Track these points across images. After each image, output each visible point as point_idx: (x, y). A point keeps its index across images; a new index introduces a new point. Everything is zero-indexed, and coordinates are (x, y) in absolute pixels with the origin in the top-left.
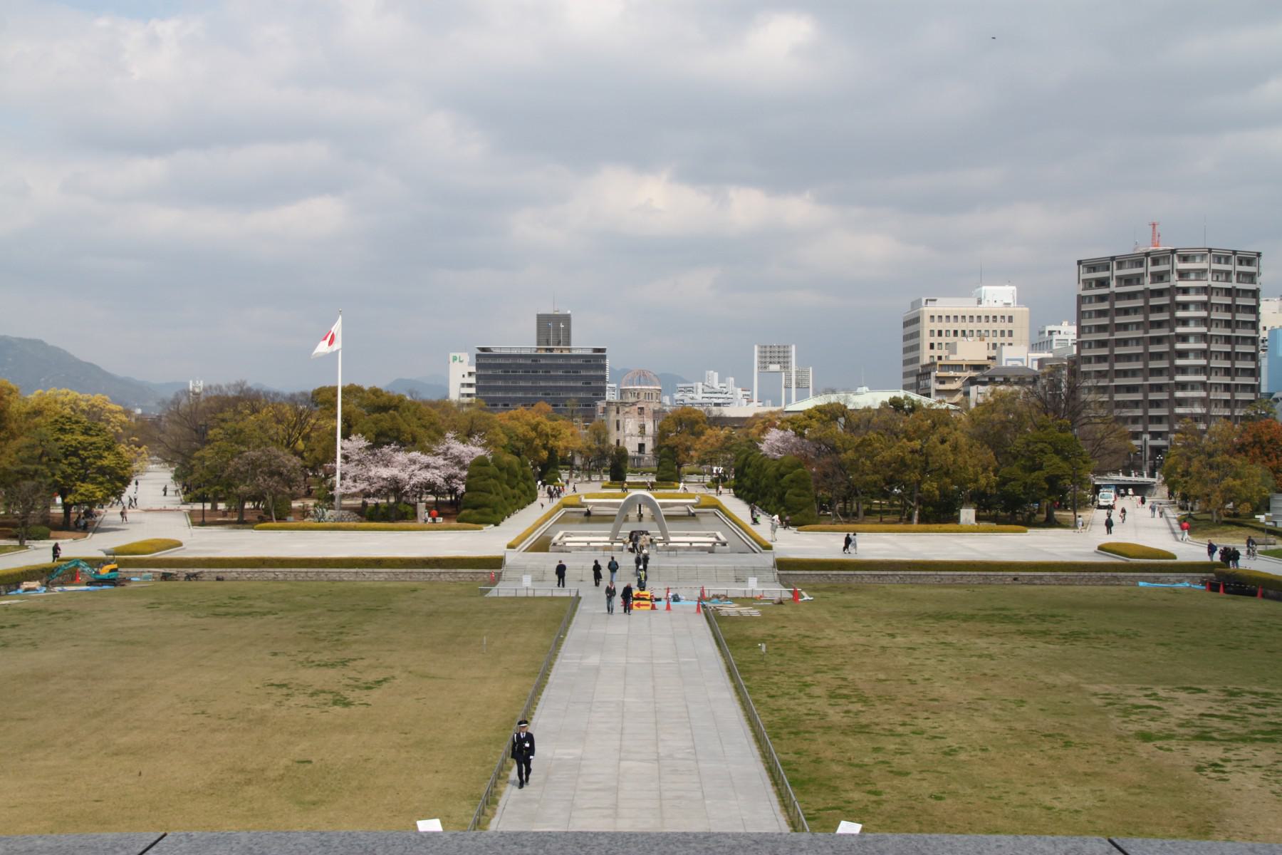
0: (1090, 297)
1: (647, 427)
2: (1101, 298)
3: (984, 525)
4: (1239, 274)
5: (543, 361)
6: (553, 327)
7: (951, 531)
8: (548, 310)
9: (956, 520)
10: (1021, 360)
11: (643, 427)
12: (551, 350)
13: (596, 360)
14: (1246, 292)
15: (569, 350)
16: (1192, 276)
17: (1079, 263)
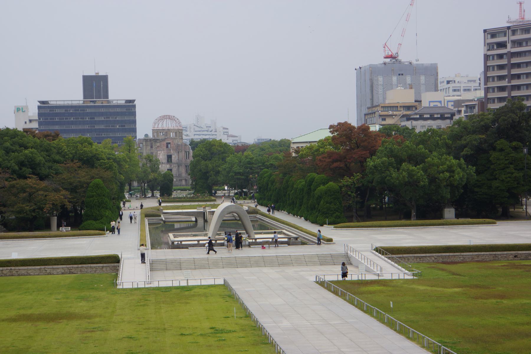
0: (493, 56)
1: (173, 157)
2: (501, 56)
3: (461, 220)
5: (88, 110)
6: (95, 85)
7: (95, 235)
9: (441, 217)
10: (440, 102)
11: (169, 157)
13: (129, 107)
15: (109, 102)
16: (524, 44)
17: (485, 31)
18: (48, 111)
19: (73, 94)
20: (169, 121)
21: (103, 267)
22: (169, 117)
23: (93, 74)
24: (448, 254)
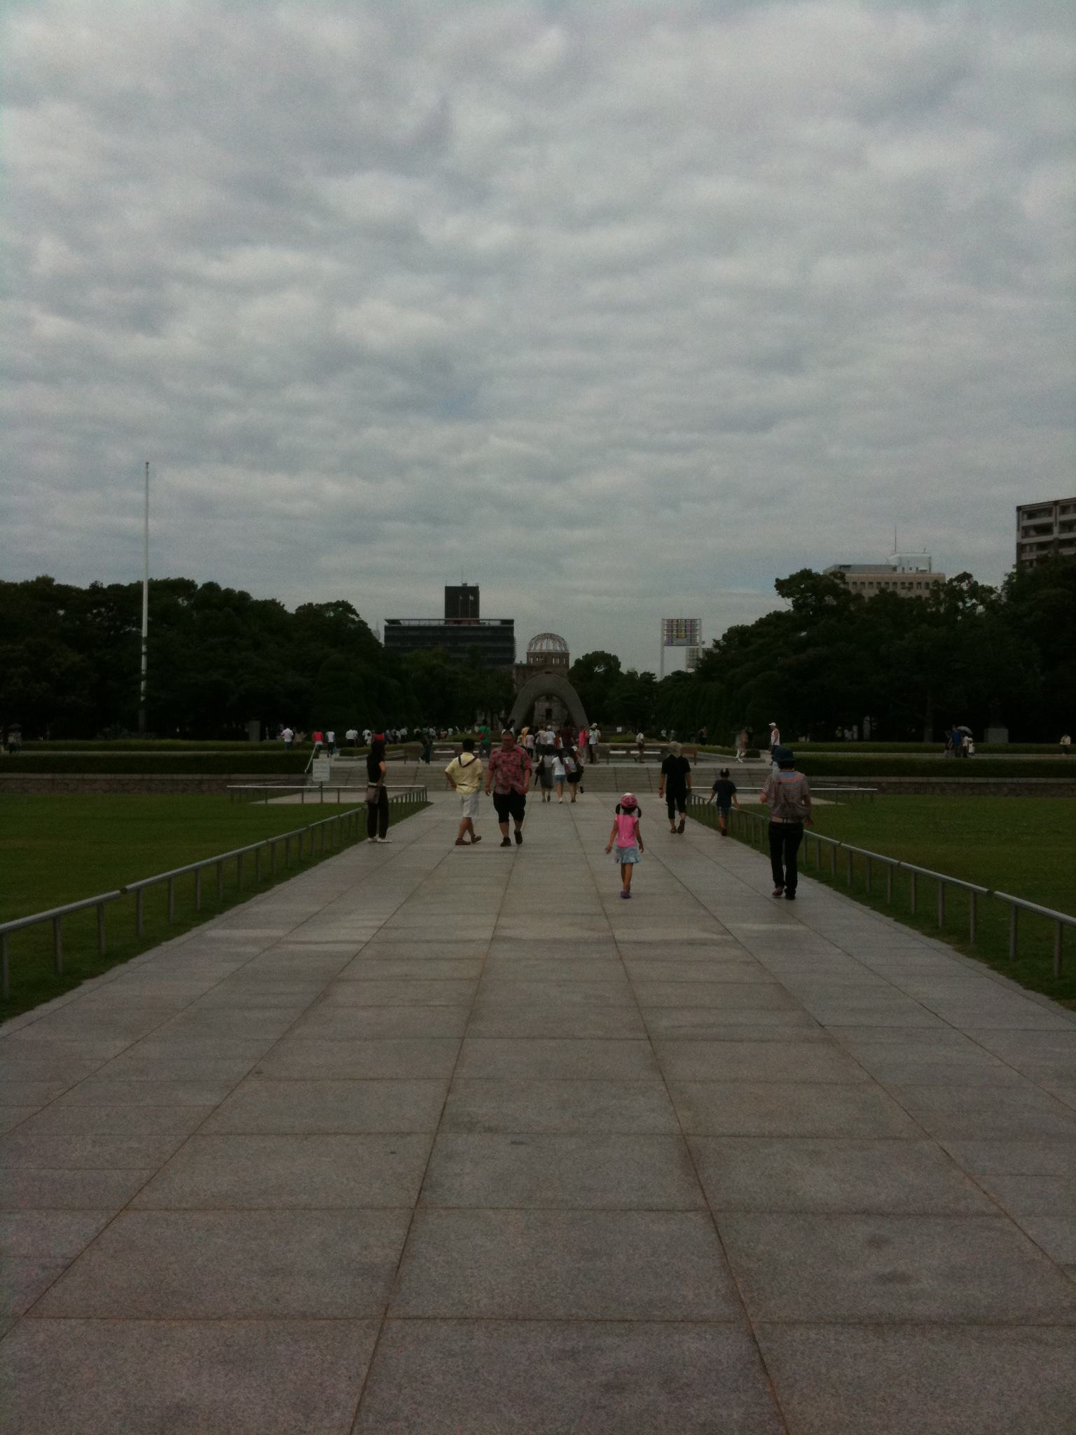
0: (1031, 545)
2: (1042, 546)
6: (462, 600)
13: (508, 625)
17: (1019, 509)
20: (551, 642)
21: (201, 782)
22: (551, 636)
23: (460, 585)
24: (1043, 780)
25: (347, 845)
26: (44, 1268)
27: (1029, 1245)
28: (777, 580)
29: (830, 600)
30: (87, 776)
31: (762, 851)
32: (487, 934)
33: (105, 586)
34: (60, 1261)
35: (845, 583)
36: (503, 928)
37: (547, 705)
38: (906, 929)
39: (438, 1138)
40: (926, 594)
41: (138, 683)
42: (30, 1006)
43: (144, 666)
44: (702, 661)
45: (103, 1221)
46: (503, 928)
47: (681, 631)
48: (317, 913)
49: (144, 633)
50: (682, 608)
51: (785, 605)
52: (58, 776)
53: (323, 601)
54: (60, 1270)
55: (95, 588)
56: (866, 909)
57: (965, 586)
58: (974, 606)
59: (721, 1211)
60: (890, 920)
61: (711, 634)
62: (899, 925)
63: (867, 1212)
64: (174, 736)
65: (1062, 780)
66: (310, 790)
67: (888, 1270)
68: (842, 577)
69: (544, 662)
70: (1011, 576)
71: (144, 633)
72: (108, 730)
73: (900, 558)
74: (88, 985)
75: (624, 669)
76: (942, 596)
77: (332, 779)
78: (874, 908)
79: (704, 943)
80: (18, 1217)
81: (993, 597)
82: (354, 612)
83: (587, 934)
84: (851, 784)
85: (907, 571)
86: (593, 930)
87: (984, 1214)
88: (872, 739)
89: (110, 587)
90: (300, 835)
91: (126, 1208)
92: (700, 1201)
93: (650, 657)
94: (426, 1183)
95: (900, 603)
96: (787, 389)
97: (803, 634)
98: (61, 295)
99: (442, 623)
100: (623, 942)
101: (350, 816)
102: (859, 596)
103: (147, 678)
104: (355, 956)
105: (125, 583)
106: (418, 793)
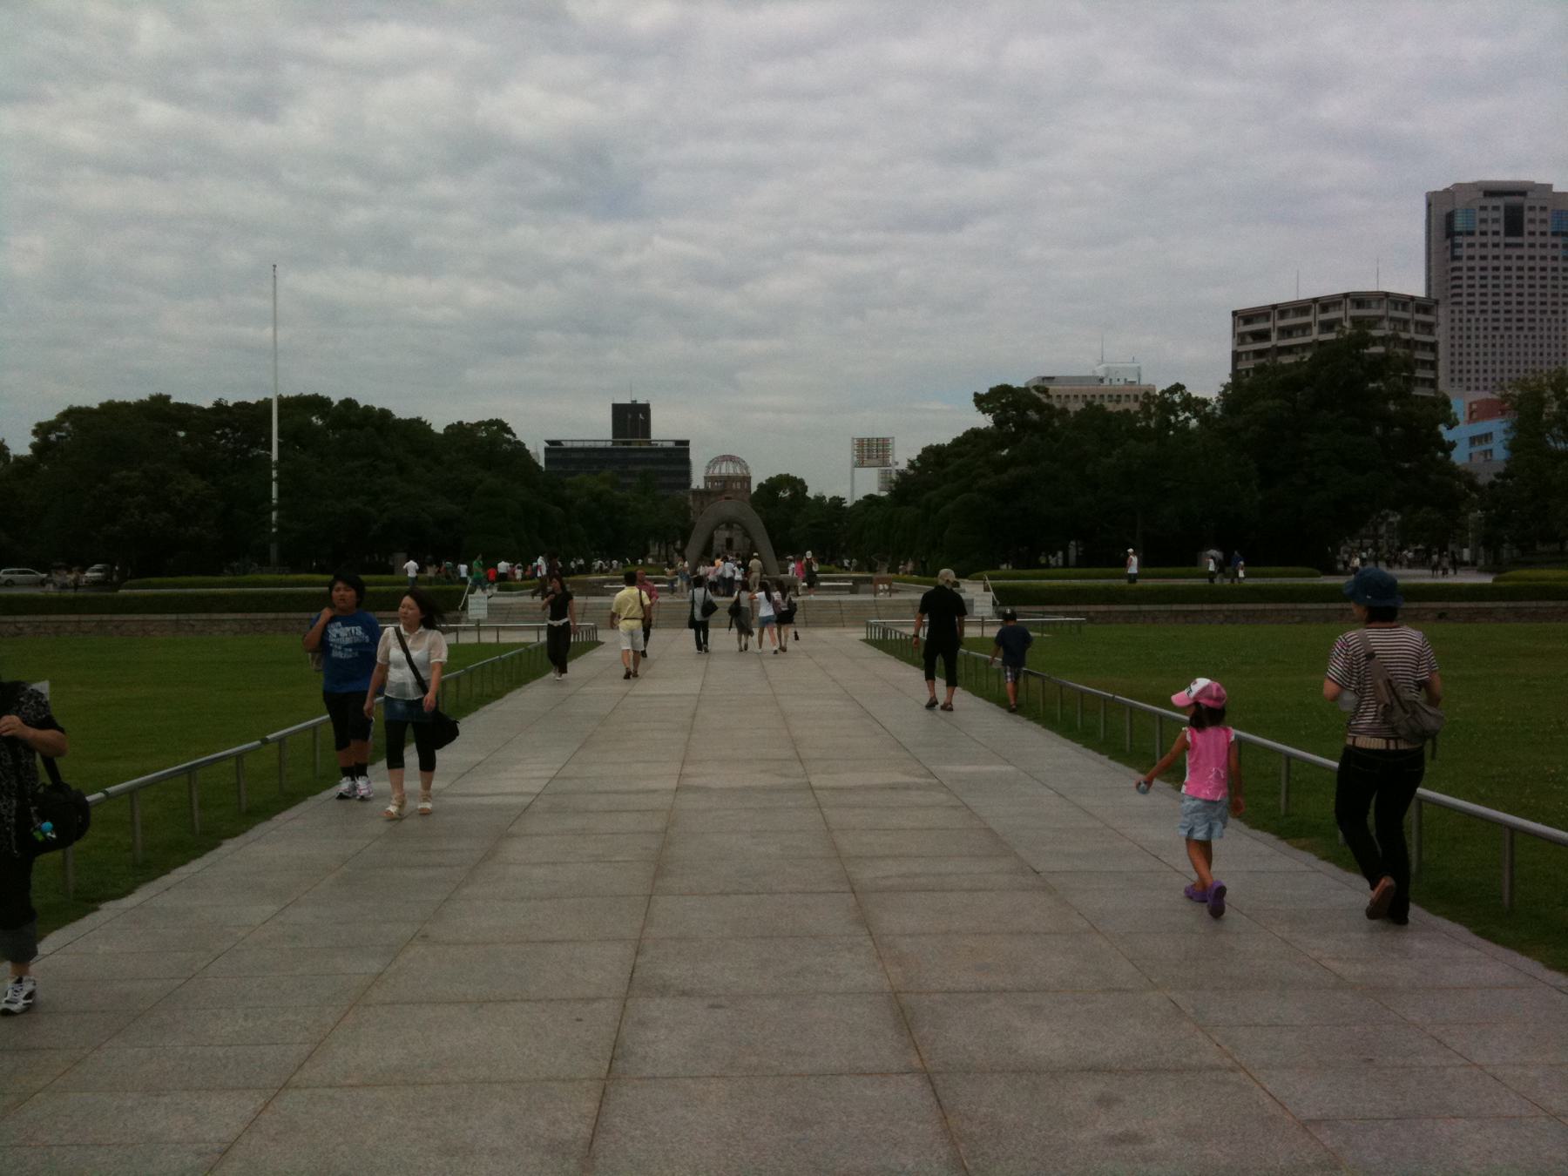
0: (1247, 353)
2: (1259, 354)
4: (1417, 323)
6: (631, 418)
8: (625, 400)
12: (629, 443)
13: (683, 446)
14: (1424, 345)
16: (1374, 304)
17: (1235, 313)
18: (559, 456)
19: (595, 427)
23: (628, 401)
25: (510, 689)
26: (199, 1154)
27: (1268, 1100)
28: (976, 394)
29: (1033, 415)
30: (216, 616)
31: (916, 665)
32: (673, 784)
33: (230, 404)
34: (216, 1146)
35: (1049, 397)
36: (688, 776)
37: (727, 534)
38: (1119, 766)
39: (629, 1003)
40: (1134, 407)
41: (270, 513)
42: (165, 870)
43: (274, 494)
44: (897, 483)
45: (262, 1101)
46: (688, 776)
47: (871, 451)
48: (479, 763)
49: (275, 456)
50: (872, 425)
51: (985, 421)
52: (182, 617)
53: (473, 421)
54: (217, 1156)
55: (220, 407)
56: (1079, 746)
57: (1177, 398)
58: (1187, 419)
59: (939, 1073)
60: (1105, 758)
61: (904, 455)
62: (1113, 763)
63: (1095, 1070)
64: (311, 571)
65: (1282, 606)
66: (465, 629)
67: (1120, 1130)
68: (1045, 391)
69: (726, 486)
70: (1226, 387)
71: (275, 456)
72: (236, 564)
73: (1108, 369)
74: (228, 846)
75: (811, 494)
76: (1153, 409)
77: (498, 615)
78: (1086, 746)
79: (907, 787)
80: (167, 1100)
81: (1208, 409)
82: (509, 431)
83: (781, 781)
84: (1056, 613)
85: (1115, 382)
86: (786, 776)
87: (1218, 1068)
88: (1078, 565)
89: (236, 405)
90: (457, 678)
91: (285, 1086)
92: (916, 1062)
93: (840, 480)
94: (617, 1051)
95: (1108, 417)
96: (981, 184)
97: (1005, 452)
98: (166, 79)
99: (609, 444)
100: (821, 789)
101: (512, 657)
102: (1064, 411)
103: (279, 507)
104: (526, 809)
105: (252, 400)
106: (588, 632)
